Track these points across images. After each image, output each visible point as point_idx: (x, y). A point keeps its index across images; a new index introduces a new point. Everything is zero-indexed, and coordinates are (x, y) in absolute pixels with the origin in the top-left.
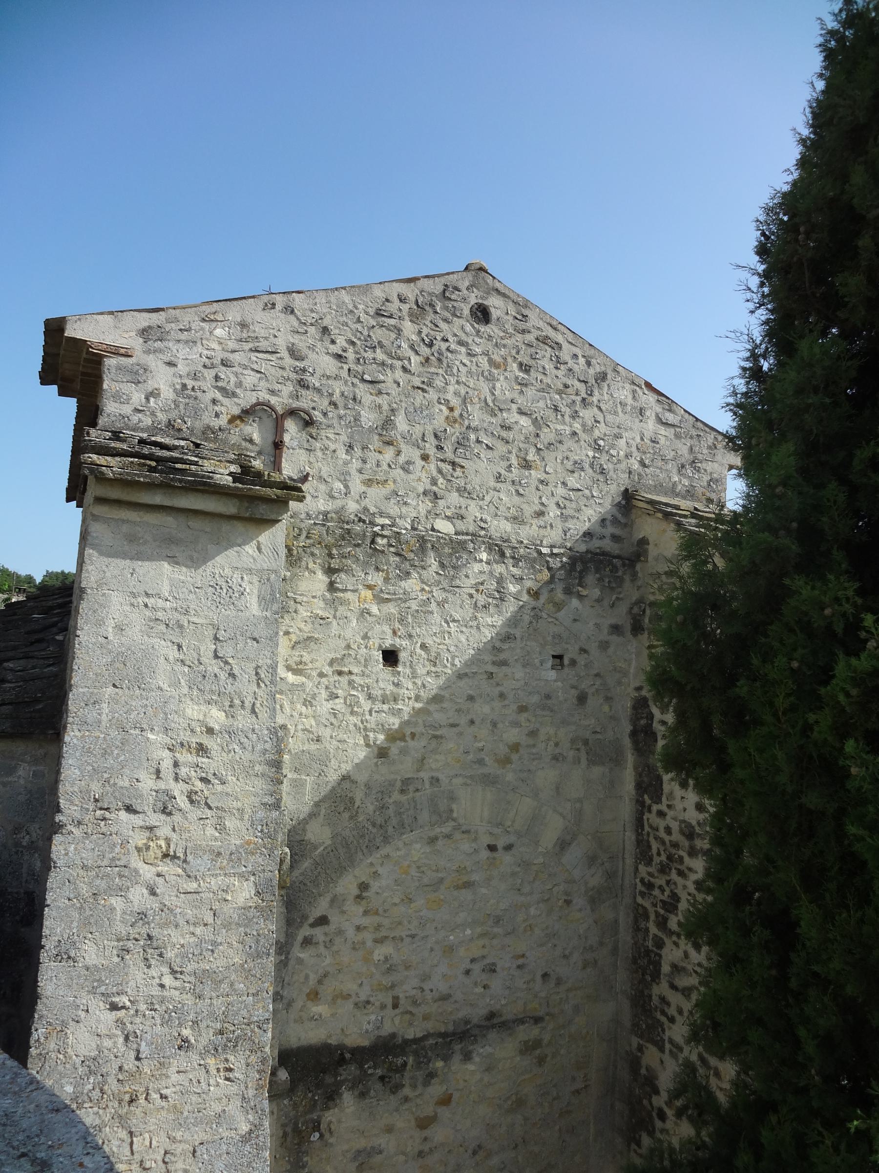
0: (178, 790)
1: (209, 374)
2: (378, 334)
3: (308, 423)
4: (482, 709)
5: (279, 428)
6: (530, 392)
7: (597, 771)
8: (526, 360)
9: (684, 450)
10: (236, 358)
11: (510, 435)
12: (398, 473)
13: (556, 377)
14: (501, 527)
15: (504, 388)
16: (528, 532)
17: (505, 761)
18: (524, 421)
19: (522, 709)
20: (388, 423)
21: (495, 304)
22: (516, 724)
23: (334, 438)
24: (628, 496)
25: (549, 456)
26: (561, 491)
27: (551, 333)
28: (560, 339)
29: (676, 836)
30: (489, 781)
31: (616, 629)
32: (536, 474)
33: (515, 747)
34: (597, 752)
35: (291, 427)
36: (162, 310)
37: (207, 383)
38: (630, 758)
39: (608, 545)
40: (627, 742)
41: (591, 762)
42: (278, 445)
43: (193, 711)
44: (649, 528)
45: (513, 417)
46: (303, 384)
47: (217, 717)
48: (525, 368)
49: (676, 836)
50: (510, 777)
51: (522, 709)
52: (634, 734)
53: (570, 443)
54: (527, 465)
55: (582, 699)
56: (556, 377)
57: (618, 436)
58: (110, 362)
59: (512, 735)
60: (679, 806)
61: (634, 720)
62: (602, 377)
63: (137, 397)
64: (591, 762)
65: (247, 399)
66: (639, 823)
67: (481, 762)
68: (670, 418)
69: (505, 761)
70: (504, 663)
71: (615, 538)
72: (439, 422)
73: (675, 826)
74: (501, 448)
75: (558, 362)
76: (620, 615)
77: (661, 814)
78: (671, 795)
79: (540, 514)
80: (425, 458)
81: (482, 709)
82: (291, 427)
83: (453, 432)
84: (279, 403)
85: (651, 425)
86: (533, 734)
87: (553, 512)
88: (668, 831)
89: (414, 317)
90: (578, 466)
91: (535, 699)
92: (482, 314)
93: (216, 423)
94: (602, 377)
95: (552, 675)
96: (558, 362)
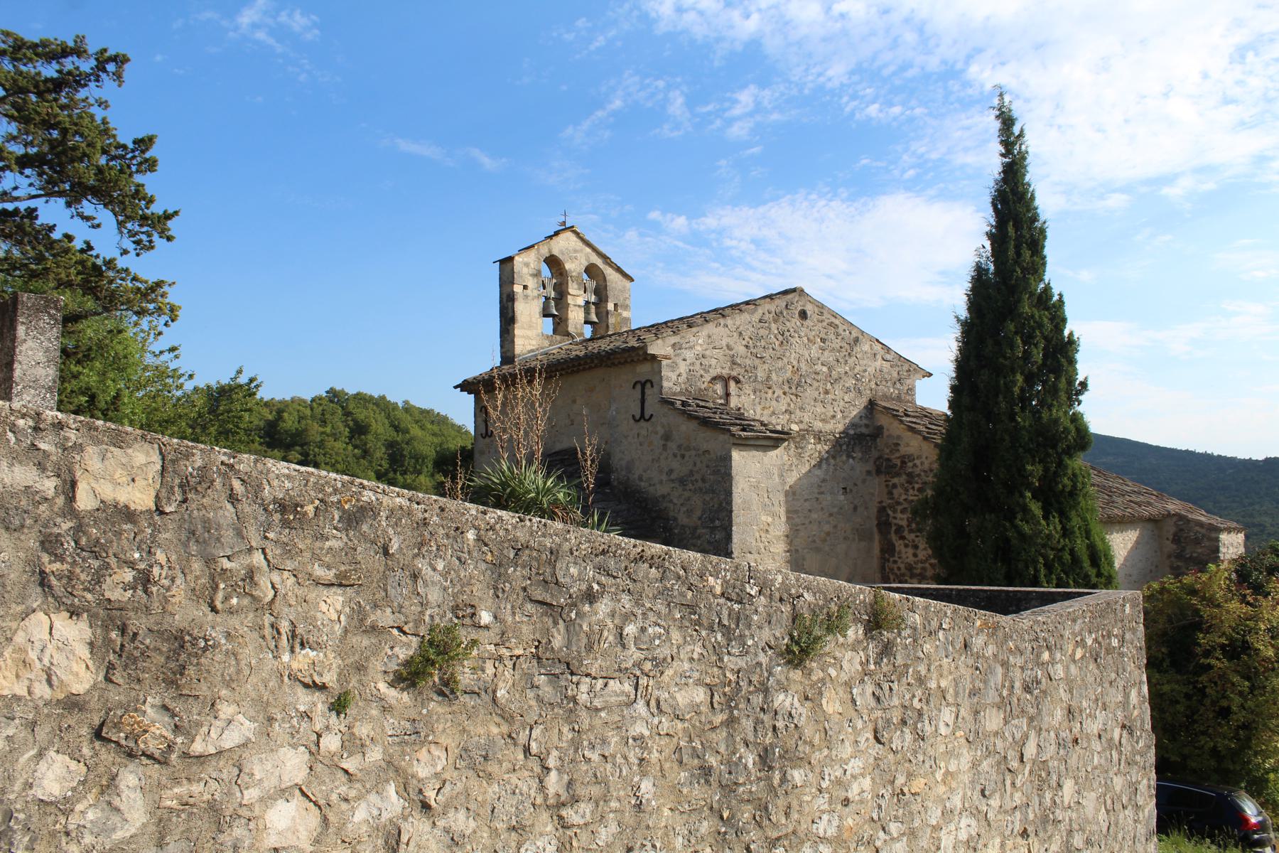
0: (762, 546)
1: (698, 363)
2: (762, 332)
3: (738, 381)
4: (814, 516)
5: (726, 387)
6: (826, 353)
7: (863, 544)
8: (823, 336)
9: (895, 374)
10: (707, 353)
11: (818, 378)
12: (774, 403)
13: (837, 343)
14: (818, 425)
15: (815, 351)
16: (828, 427)
17: (825, 540)
18: (825, 369)
19: (831, 515)
20: (768, 378)
21: (809, 309)
22: (828, 522)
23: (748, 389)
24: (872, 405)
25: (836, 386)
26: (842, 403)
27: (833, 320)
28: (837, 322)
29: (903, 570)
30: (818, 550)
31: (869, 473)
32: (830, 396)
33: (828, 534)
34: (863, 535)
35: (732, 384)
36: (533, 246)
37: (697, 367)
38: (877, 537)
39: (864, 430)
40: (875, 530)
41: (860, 540)
42: (728, 395)
43: (764, 518)
44: (883, 420)
45: (819, 367)
46: (734, 363)
47: (770, 520)
48: (823, 340)
49: (903, 570)
50: (827, 548)
51: (831, 515)
52: (878, 525)
53: (845, 378)
54: (827, 392)
55: (855, 508)
56: (837, 343)
57: (865, 371)
58: (664, 362)
59: (827, 528)
60: (904, 556)
61: (878, 518)
62: (856, 340)
63: (674, 377)
64: (860, 540)
65: (713, 373)
66: (883, 568)
67: (814, 541)
68: (888, 357)
69: (825, 540)
70: (822, 493)
71: (867, 426)
72: (789, 374)
73: (902, 566)
74: (816, 384)
75: (838, 335)
76: (870, 466)
77: (895, 562)
78: (900, 552)
79: (834, 417)
80: (785, 393)
81: (814, 516)
82: (732, 384)
83: (796, 378)
84: (725, 372)
85: (879, 363)
86: (835, 527)
87: (839, 415)
88: (899, 569)
89: (775, 321)
90: (848, 390)
91: (836, 510)
92: (803, 315)
93: (703, 387)
94: (856, 340)
95: (842, 497)
96: (838, 335)
